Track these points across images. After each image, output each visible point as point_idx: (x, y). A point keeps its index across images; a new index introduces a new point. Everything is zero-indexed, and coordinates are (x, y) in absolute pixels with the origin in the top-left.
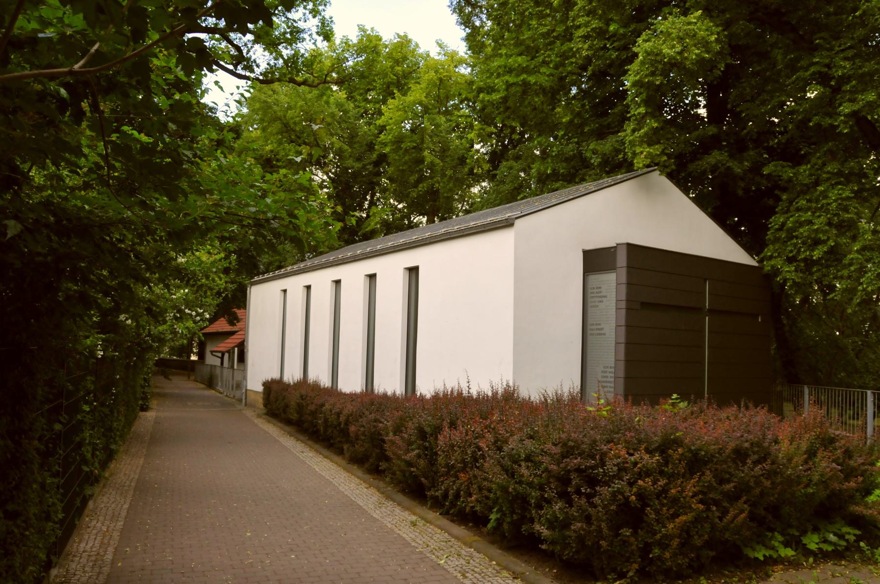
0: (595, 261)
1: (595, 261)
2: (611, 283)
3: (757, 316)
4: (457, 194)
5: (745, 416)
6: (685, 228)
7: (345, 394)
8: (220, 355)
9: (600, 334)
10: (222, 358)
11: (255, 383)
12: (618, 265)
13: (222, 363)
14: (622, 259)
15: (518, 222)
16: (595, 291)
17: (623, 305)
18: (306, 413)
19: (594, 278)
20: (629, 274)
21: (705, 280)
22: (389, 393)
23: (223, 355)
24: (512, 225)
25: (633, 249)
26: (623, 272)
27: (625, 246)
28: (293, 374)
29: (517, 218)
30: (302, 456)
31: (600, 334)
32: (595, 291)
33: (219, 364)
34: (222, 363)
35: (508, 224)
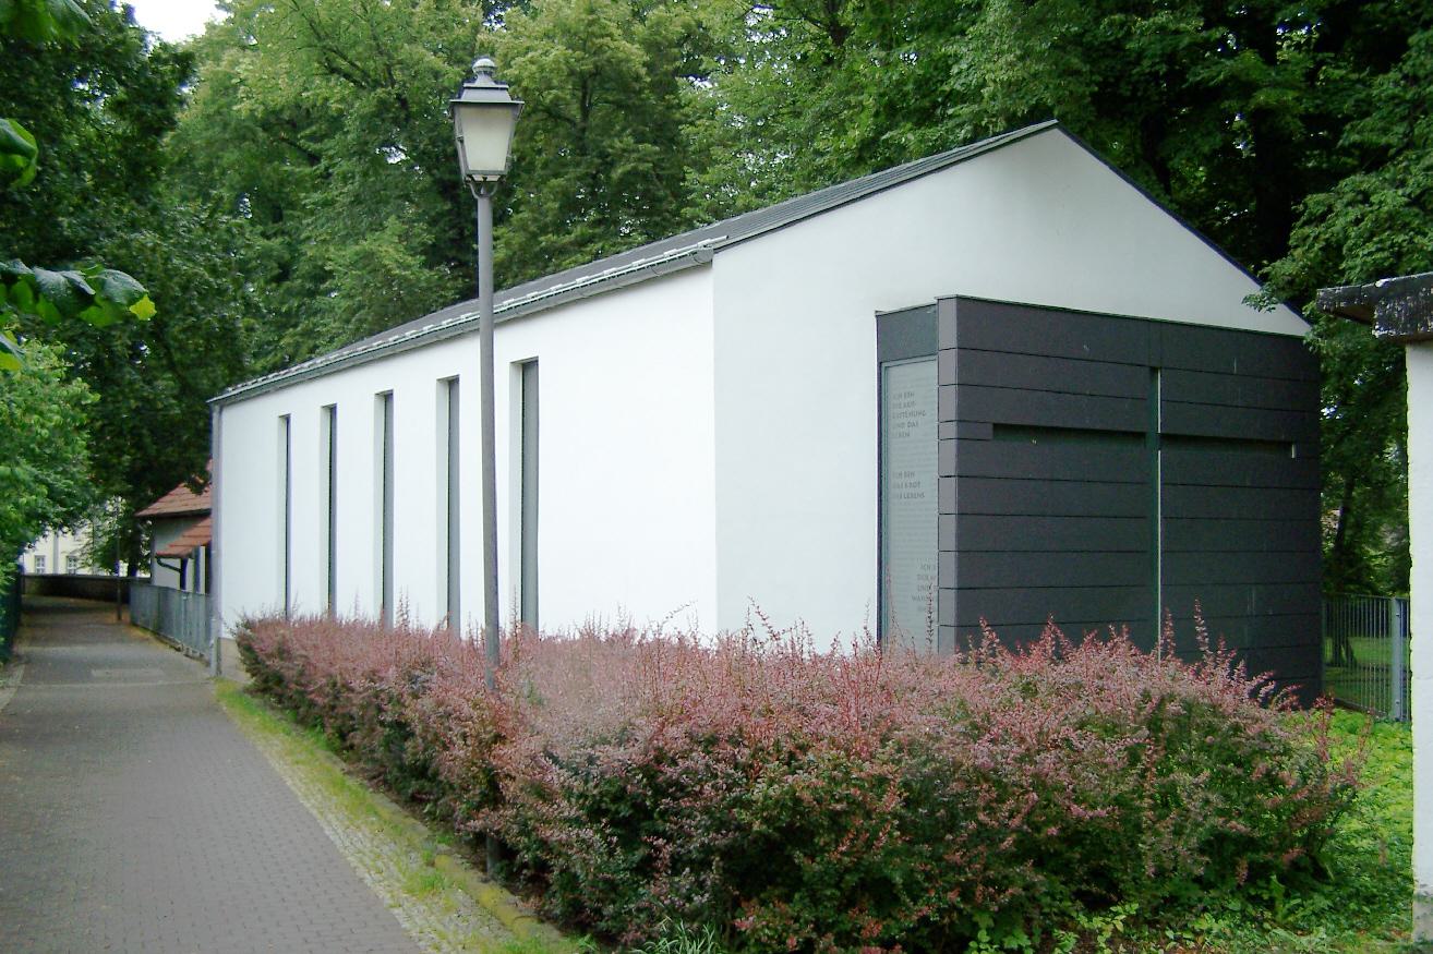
0: (900, 335)
1: (900, 335)
2: (929, 385)
3: (1286, 446)
4: (1220, 205)
5: (1086, 661)
6: (1135, 260)
7: (568, 644)
8: (177, 563)
9: (913, 496)
10: (182, 571)
11: (229, 620)
12: (942, 345)
13: (183, 584)
14: (948, 331)
15: (720, 260)
16: (903, 401)
17: (952, 430)
18: (292, 679)
19: (903, 374)
20: (962, 365)
21: (1154, 370)
22: (708, 639)
23: (184, 564)
24: (707, 265)
25: (969, 307)
26: (950, 359)
27: (954, 301)
28: (309, 604)
29: (717, 250)
30: (278, 766)
31: (913, 496)
32: (903, 401)
33: (177, 586)
34: (183, 584)
35: (700, 264)
